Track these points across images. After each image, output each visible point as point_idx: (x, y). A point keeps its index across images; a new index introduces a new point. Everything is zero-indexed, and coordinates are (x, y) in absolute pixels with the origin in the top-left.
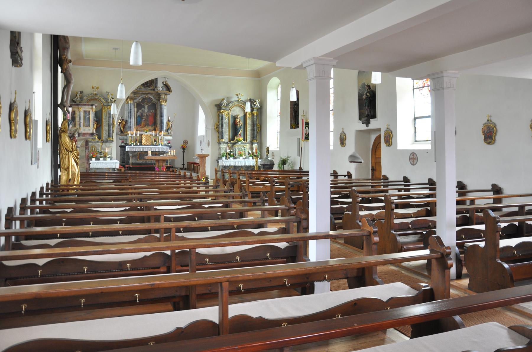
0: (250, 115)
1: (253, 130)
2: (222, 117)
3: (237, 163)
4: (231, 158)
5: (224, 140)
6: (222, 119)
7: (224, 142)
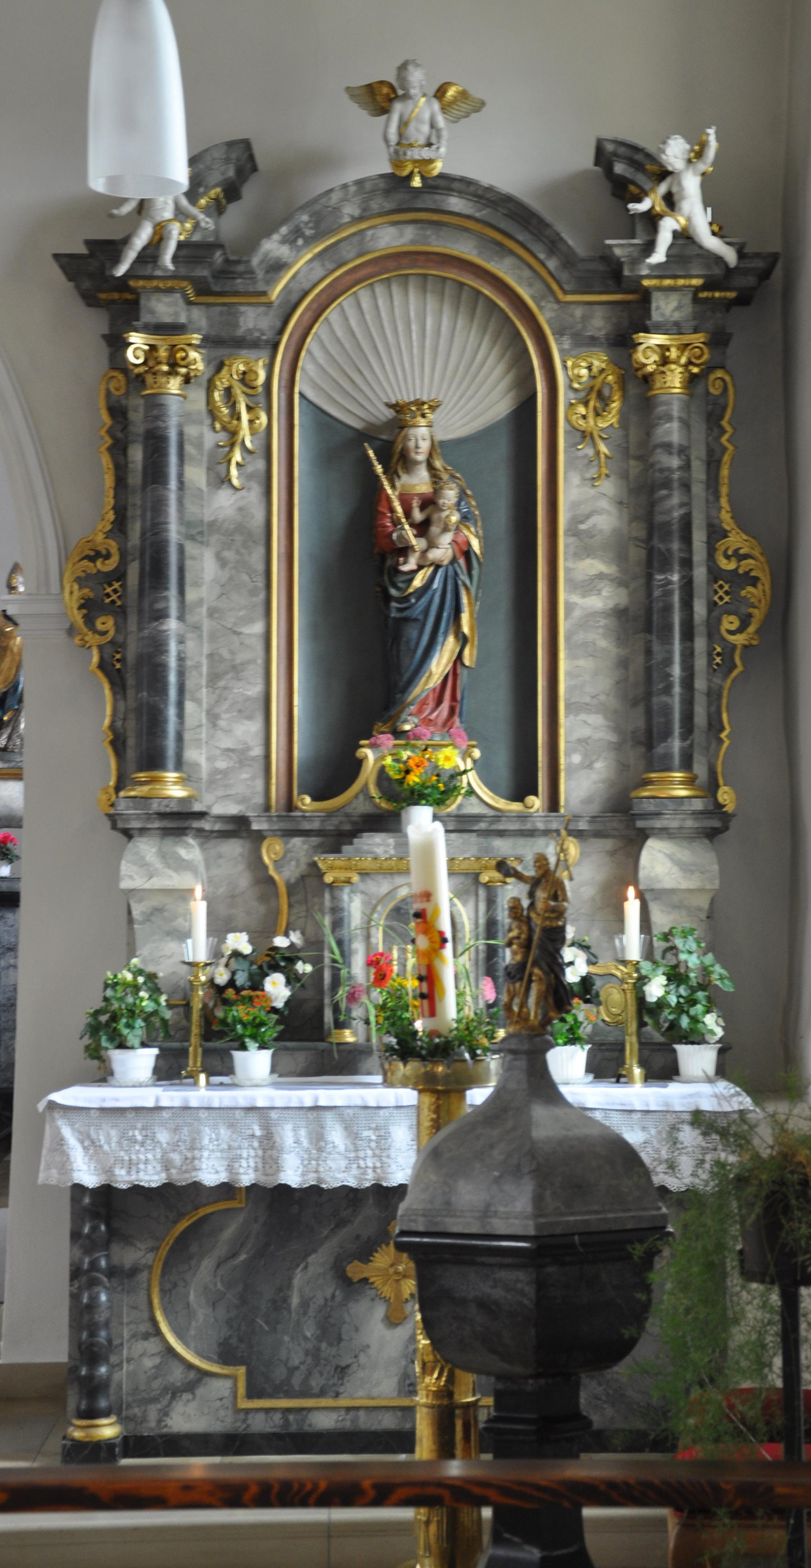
0: (595, 396)
1: (642, 623)
2: (156, 443)
3: (291, 1137)
4: (255, 1062)
5: (173, 788)
6: (155, 472)
7: (179, 821)
